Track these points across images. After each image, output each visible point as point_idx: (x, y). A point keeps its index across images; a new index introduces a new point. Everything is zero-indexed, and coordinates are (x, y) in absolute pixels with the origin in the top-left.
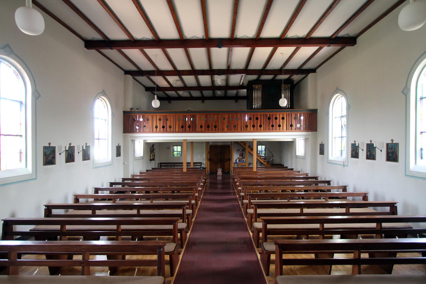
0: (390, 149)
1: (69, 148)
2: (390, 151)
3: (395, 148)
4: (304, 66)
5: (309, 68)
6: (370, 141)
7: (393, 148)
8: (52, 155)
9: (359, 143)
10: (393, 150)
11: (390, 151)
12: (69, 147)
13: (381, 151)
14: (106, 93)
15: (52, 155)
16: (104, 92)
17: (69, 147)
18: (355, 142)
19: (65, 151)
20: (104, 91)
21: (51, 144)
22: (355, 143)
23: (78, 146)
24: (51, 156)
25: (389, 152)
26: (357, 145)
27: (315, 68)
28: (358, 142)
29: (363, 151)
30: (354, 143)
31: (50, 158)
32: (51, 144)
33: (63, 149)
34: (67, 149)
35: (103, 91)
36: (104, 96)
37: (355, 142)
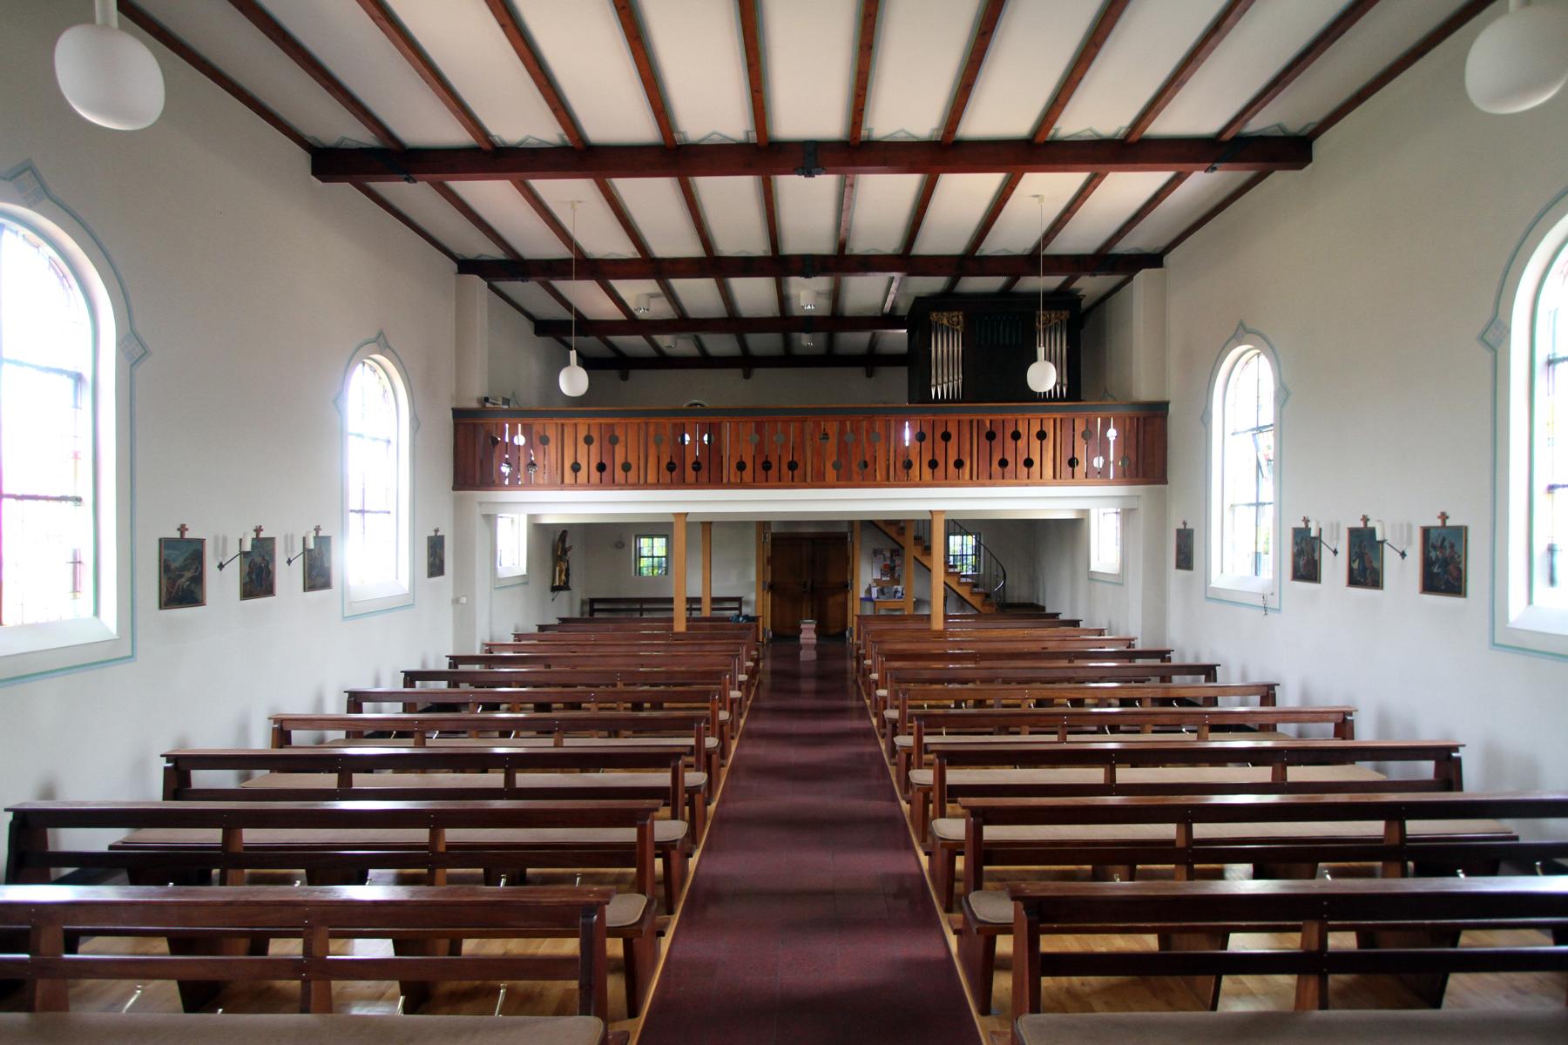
0: (1434, 547)
1: (253, 546)
2: (1437, 556)
3: (1452, 546)
4: (1118, 245)
5: (1138, 249)
6: (1362, 520)
7: (1447, 544)
8: (192, 571)
9: (1321, 526)
10: (1448, 551)
11: (1437, 556)
12: (253, 539)
13: (1403, 555)
14: (391, 344)
15: (192, 571)
16: (381, 340)
17: (253, 539)
18: (1306, 521)
19: (240, 554)
20: (384, 337)
21: (187, 530)
22: (1307, 525)
23: (286, 537)
24: (188, 574)
25: (1431, 558)
26: (1313, 533)
27: (1158, 251)
28: (1318, 523)
29: (1338, 555)
30: (1302, 525)
31: (183, 580)
32: (187, 530)
33: (234, 550)
34: (248, 547)
35: (379, 336)
36: (381, 354)
37: (1308, 521)
